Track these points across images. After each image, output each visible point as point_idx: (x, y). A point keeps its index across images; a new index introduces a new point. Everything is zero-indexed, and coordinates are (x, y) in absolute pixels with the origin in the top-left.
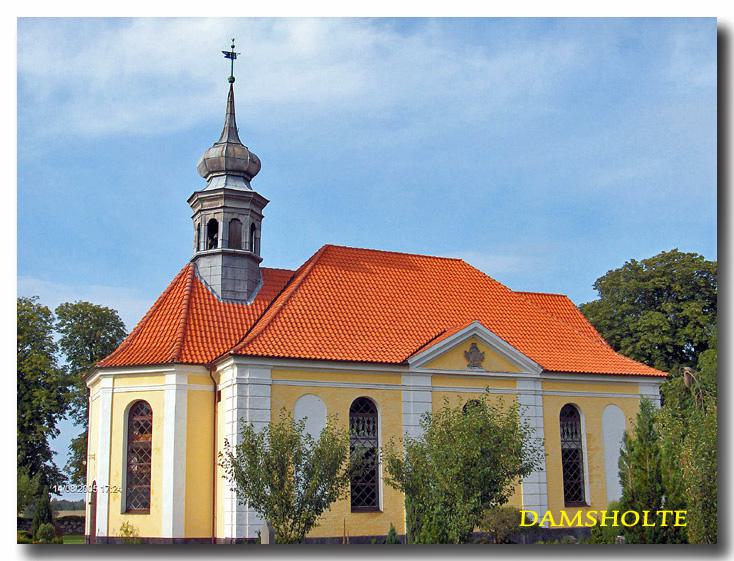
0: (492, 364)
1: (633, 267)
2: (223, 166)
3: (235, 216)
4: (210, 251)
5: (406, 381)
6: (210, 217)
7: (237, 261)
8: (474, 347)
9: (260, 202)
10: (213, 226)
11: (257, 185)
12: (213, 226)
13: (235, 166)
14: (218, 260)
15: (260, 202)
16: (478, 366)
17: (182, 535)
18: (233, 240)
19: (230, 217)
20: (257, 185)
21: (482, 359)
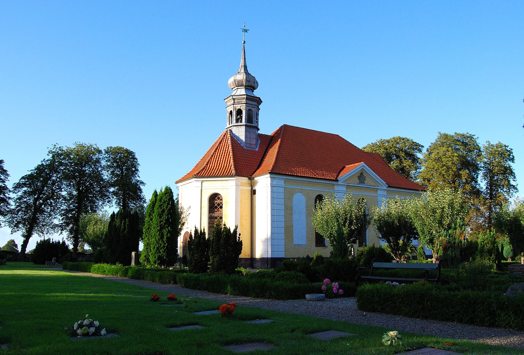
0: (368, 181)
1: (382, 142)
2: (244, 84)
3: (250, 108)
4: (237, 124)
5: (336, 188)
6: (238, 108)
7: (251, 129)
8: (362, 174)
9: (259, 101)
10: (239, 112)
11: (256, 93)
12: (239, 112)
13: (249, 84)
14: (243, 128)
15: (259, 101)
16: (364, 183)
17: (282, 255)
18: (250, 119)
19: (248, 108)
20: (256, 93)
21: (365, 179)
